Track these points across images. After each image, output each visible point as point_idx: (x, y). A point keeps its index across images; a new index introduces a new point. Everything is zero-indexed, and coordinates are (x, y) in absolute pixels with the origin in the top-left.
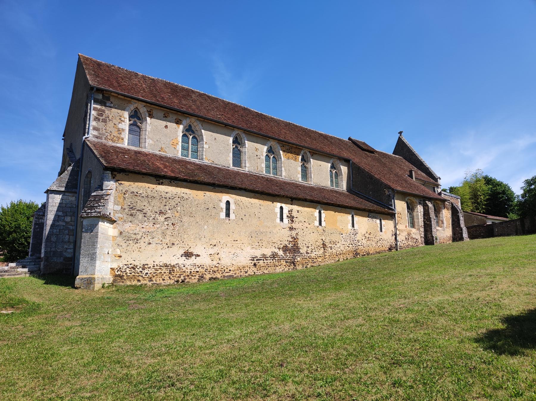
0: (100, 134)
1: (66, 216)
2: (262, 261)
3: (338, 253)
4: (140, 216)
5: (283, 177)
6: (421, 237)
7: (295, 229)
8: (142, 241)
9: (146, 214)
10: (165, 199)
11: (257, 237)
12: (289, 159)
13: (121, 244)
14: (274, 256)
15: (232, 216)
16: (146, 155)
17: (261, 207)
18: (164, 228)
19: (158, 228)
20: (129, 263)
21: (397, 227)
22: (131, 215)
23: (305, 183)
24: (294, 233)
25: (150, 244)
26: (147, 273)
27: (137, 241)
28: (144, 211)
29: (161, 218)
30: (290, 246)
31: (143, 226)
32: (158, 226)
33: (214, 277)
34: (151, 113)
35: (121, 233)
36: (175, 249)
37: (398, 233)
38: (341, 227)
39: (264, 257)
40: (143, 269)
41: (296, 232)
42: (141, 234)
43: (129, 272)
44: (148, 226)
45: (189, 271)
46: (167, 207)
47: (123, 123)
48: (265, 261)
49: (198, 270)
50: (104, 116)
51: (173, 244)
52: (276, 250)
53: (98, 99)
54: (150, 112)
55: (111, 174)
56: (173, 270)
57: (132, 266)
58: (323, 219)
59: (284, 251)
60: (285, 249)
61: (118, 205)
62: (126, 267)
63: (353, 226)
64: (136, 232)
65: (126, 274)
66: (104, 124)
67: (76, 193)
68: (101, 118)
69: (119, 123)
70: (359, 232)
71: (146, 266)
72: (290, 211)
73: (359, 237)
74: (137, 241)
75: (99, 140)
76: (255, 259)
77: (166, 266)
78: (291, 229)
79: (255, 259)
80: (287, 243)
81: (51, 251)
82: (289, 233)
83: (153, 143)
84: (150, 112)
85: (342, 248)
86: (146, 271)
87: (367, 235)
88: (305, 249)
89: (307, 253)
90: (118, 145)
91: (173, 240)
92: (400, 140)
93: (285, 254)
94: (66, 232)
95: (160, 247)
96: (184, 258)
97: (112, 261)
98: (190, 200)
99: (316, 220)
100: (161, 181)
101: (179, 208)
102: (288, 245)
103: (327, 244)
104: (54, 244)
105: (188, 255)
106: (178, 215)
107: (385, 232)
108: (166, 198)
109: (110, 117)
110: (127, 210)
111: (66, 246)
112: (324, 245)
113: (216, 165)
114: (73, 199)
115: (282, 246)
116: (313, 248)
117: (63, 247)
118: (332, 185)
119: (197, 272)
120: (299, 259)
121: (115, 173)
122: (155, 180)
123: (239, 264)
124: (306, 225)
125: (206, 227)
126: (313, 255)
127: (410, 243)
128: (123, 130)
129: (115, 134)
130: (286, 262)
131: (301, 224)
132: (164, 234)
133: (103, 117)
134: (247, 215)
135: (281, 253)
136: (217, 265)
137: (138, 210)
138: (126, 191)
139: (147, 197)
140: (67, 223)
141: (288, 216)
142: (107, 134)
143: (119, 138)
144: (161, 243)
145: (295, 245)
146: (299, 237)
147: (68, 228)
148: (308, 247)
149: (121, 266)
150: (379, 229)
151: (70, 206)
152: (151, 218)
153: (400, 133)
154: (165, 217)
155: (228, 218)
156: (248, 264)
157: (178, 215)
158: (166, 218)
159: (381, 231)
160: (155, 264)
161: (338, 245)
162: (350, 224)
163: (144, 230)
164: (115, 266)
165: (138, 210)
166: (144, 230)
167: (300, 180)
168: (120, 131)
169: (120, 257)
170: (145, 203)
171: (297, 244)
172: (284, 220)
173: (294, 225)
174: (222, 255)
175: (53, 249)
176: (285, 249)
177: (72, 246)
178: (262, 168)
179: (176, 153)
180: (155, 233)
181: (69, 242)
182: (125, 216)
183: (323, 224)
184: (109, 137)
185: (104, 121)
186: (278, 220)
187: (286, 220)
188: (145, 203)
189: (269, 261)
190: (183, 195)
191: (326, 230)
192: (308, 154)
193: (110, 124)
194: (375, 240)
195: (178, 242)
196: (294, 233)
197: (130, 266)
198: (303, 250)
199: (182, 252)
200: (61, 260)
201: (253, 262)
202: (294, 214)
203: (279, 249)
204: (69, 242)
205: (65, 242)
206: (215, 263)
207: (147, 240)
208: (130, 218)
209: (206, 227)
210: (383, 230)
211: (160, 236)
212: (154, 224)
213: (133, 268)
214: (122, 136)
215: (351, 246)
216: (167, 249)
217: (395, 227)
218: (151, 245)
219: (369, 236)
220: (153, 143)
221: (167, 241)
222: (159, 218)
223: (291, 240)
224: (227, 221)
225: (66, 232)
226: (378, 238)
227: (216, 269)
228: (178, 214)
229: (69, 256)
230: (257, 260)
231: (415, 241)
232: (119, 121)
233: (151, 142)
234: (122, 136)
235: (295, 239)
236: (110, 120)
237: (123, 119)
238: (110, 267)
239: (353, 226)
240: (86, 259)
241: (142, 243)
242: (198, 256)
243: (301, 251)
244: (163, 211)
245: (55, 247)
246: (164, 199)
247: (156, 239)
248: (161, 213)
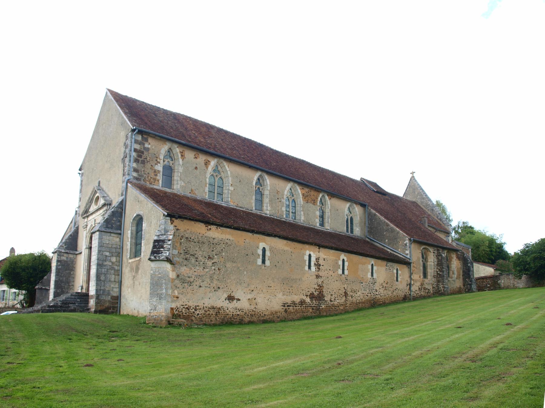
0: (139, 175)
1: (112, 256)
2: (292, 307)
3: (358, 301)
4: (193, 260)
5: (302, 221)
6: (433, 287)
7: (321, 277)
8: (194, 284)
9: (197, 258)
10: (213, 243)
11: (288, 282)
12: (307, 203)
13: (178, 286)
14: (302, 302)
15: (268, 263)
16: (175, 195)
17: (292, 254)
18: (211, 272)
19: (207, 272)
20: (184, 304)
21: (412, 277)
22: (186, 259)
23: (321, 228)
24: (320, 281)
25: (200, 287)
26: (198, 314)
27: (190, 283)
28: (196, 256)
29: (209, 263)
30: (316, 294)
31: (195, 270)
32: (207, 270)
33: (252, 320)
34: (183, 154)
35: (178, 276)
36: (220, 292)
37: (412, 283)
38: (361, 276)
39: (294, 303)
40: (196, 310)
41: (322, 280)
42: (193, 278)
43: (184, 312)
44: (199, 270)
45: (231, 314)
46: (214, 253)
47: (159, 164)
48: (295, 308)
49: (238, 313)
50: (143, 157)
51: (219, 288)
52: (304, 297)
53: (138, 141)
54: (182, 152)
55: (171, 220)
56: (219, 312)
57: (187, 306)
58: (346, 268)
59: (310, 298)
60: (312, 296)
61: (175, 249)
62: (182, 307)
63: (372, 275)
64: (190, 275)
65: (182, 313)
66: (142, 165)
67: (120, 234)
68: (140, 159)
69: (156, 164)
70: (378, 281)
71: (198, 307)
72: (317, 259)
73: (377, 286)
74: (190, 283)
75: (139, 182)
76: (286, 305)
77: (213, 308)
78: (318, 277)
79: (286, 305)
80: (313, 290)
81: (100, 290)
82: (316, 281)
83: (184, 185)
84: (182, 152)
85: (362, 297)
86: (197, 312)
87: (384, 285)
88: (329, 296)
89: (331, 301)
90: (155, 187)
91: (219, 284)
92: (413, 179)
93: (312, 301)
94: (113, 271)
95: (208, 290)
96: (227, 301)
97: (172, 302)
98: (232, 246)
99: (339, 268)
100: (209, 227)
101: (224, 254)
102: (314, 293)
103: (348, 293)
104: (103, 283)
105: (231, 298)
106: (222, 260)
107: (401, 282)
108: (213, 244)
109: (148, 158)
110: (182, 255)
111: (112, 286)
112: (346, 294)
113: (241, 207)
114: (118, 240)
115: (309, 294)
116: (336, 296)
117: (110, 286)
118: (347, 231)
119: (238, 315)
120: (323, 306)
121: (173, 219)
122: (205, 226)
123: (272, 309)
124: (331, 273)
125: (245, 273)
126: (336, 303)
127: (423, 293)
128: (159, 171)
129: (152, 175)
130: (313, 309)
131: (326, 272)
132: (211, 278)
133: (142, 159)
134: (280, 263)
135: (308, 300)
136: (254, 310)
137: (191, 255)
138: (182, 237)
139: (199, 242)
140: (113, 263)
141: (315, 264)
142: (145, 175)
143: (155, 179)
144: (209, 286)
145: (320, 292)
146: (324, 285)
147: (114, 268)
148: (332, 295)
149: (179, 306)
150: (395, 279)
151: (115, 246)
152: (201, 263)
153: (413, 173)
154: (213, 261)
155: (263, 265)
156: (280, 310)
157: (222, 260)
158: (213, 263)
159: (397, 280)
160: (205, 305)
161: (359, 293)
162: (370, 274)
163: (196, 273)
164: (174, 305)
165: (191, 255)
166: (196, 273)
167: (318, 225)
168: (156, 172)
169: (178, 298)
170: (197, 249)
171: (323, 292)
172: (312, 268)
173: (321, 273)
174: (259, 300)
175: (102, 288)
176: (312, 296)
177: (117, 285)
178: (283, 212)
179: (204, 195)
180: (204, 277)
181: (115, 281)
182: (181, 260)
183: (346, 272)
184: (147, 179)
185: (143, 162)
186: (307, 268)
187: (313, 268)
188: (197, 249)
189: (298, 308)
190: (228, 241)
191: (348, 278)
192: (327, 197)
193: (148, 166)
194: (392, 289)
195: (223, 286)
196: (320, 281)
197: (186, 307)
198: (327, 298)
199: (226, 296)
200: (109, 298)
201: (284, 308)
202: (321, 262)
203: (307, 296)
204: (115, 281)
205: (112, 282)
206: (252, 307)
207: (198, 283)
208: (185, 262)
209: (245, 273)
210: (399, 279)
211: (208, 280)
212: (204, 268)
213: (187, 308)
214: (158, 178)
215: (369, 295)
216: (214, 293)
217: (410, 277)
218: (201, 289)
219: (387, 286)
220: (184, 185)
221: (214, 285)
222: (208, 263)
223: (318, 288)
224: (263, 267)
225: (113, 271)
226: (394, 288)
227: (253, 313)
228: (223, 259)
229: (115, 295)
230: (288, 306)
231: (427, 291)
232: (156, 162)
233: (183, 184)
234: (158, 178)
235: (320, 286)
236: (148, 162)
237: (158, 160)
238: (170, 307)
239: (372, 275)
240: (155, 299)
241: (194, 285)
242: (239, 300)
243: (326, 299)
244: (211, 256)
245: (104, 286)
246: (211, 244)
247: (205, 282)
248: (209, 258)
